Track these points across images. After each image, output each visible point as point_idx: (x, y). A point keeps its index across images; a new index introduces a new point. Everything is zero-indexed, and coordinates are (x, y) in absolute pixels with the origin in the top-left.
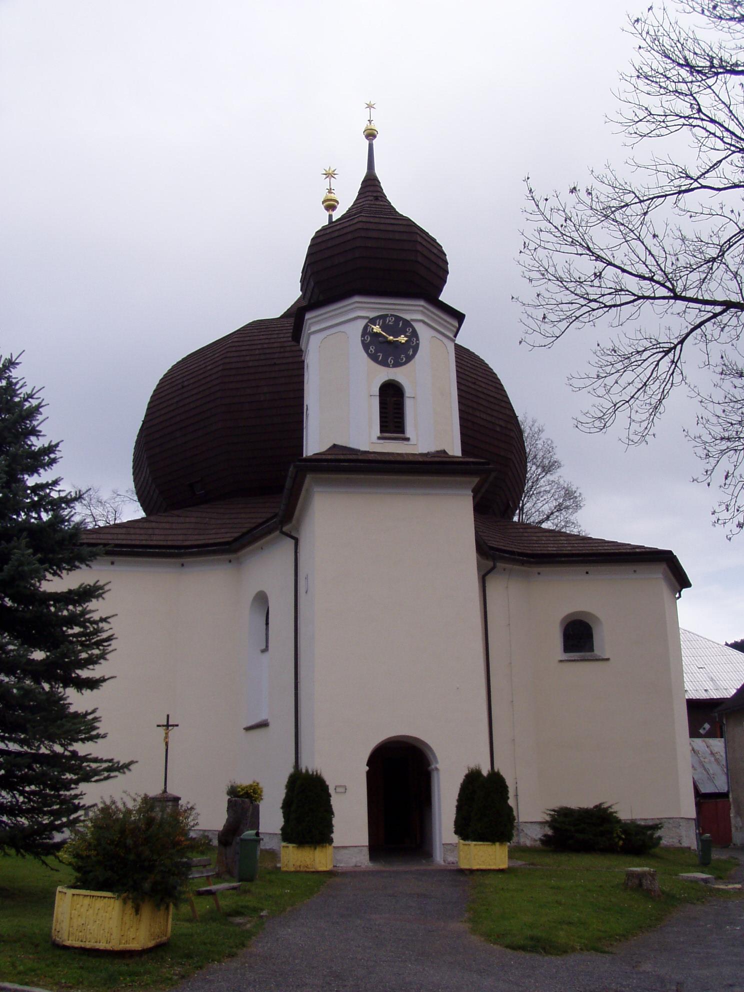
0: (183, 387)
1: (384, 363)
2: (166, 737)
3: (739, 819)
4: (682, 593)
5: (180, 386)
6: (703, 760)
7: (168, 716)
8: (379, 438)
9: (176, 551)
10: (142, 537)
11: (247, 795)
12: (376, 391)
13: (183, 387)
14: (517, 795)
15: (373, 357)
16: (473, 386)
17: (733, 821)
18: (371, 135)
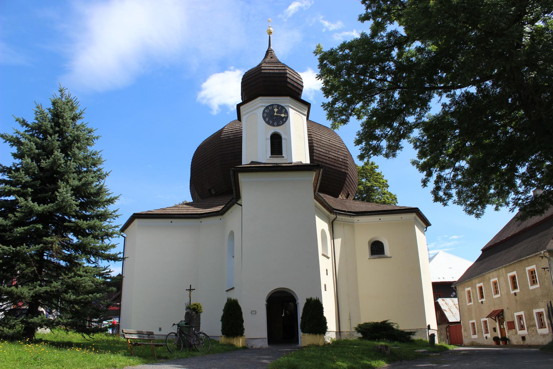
0: (205, 149)
1: (273, 125)
2: (190, 295)
3: (465, 333)
4: (427, 228)
5: (204, 149)
7: (191, 285)
8: (270, 157)
9: (520, 349)
10: (185, 211)
11: (194, 309)
12: (269, 137)
14: (350, 319)
15: (268, 123)
16: (328, 142)
17: (463, 334)
18: (270, 33)
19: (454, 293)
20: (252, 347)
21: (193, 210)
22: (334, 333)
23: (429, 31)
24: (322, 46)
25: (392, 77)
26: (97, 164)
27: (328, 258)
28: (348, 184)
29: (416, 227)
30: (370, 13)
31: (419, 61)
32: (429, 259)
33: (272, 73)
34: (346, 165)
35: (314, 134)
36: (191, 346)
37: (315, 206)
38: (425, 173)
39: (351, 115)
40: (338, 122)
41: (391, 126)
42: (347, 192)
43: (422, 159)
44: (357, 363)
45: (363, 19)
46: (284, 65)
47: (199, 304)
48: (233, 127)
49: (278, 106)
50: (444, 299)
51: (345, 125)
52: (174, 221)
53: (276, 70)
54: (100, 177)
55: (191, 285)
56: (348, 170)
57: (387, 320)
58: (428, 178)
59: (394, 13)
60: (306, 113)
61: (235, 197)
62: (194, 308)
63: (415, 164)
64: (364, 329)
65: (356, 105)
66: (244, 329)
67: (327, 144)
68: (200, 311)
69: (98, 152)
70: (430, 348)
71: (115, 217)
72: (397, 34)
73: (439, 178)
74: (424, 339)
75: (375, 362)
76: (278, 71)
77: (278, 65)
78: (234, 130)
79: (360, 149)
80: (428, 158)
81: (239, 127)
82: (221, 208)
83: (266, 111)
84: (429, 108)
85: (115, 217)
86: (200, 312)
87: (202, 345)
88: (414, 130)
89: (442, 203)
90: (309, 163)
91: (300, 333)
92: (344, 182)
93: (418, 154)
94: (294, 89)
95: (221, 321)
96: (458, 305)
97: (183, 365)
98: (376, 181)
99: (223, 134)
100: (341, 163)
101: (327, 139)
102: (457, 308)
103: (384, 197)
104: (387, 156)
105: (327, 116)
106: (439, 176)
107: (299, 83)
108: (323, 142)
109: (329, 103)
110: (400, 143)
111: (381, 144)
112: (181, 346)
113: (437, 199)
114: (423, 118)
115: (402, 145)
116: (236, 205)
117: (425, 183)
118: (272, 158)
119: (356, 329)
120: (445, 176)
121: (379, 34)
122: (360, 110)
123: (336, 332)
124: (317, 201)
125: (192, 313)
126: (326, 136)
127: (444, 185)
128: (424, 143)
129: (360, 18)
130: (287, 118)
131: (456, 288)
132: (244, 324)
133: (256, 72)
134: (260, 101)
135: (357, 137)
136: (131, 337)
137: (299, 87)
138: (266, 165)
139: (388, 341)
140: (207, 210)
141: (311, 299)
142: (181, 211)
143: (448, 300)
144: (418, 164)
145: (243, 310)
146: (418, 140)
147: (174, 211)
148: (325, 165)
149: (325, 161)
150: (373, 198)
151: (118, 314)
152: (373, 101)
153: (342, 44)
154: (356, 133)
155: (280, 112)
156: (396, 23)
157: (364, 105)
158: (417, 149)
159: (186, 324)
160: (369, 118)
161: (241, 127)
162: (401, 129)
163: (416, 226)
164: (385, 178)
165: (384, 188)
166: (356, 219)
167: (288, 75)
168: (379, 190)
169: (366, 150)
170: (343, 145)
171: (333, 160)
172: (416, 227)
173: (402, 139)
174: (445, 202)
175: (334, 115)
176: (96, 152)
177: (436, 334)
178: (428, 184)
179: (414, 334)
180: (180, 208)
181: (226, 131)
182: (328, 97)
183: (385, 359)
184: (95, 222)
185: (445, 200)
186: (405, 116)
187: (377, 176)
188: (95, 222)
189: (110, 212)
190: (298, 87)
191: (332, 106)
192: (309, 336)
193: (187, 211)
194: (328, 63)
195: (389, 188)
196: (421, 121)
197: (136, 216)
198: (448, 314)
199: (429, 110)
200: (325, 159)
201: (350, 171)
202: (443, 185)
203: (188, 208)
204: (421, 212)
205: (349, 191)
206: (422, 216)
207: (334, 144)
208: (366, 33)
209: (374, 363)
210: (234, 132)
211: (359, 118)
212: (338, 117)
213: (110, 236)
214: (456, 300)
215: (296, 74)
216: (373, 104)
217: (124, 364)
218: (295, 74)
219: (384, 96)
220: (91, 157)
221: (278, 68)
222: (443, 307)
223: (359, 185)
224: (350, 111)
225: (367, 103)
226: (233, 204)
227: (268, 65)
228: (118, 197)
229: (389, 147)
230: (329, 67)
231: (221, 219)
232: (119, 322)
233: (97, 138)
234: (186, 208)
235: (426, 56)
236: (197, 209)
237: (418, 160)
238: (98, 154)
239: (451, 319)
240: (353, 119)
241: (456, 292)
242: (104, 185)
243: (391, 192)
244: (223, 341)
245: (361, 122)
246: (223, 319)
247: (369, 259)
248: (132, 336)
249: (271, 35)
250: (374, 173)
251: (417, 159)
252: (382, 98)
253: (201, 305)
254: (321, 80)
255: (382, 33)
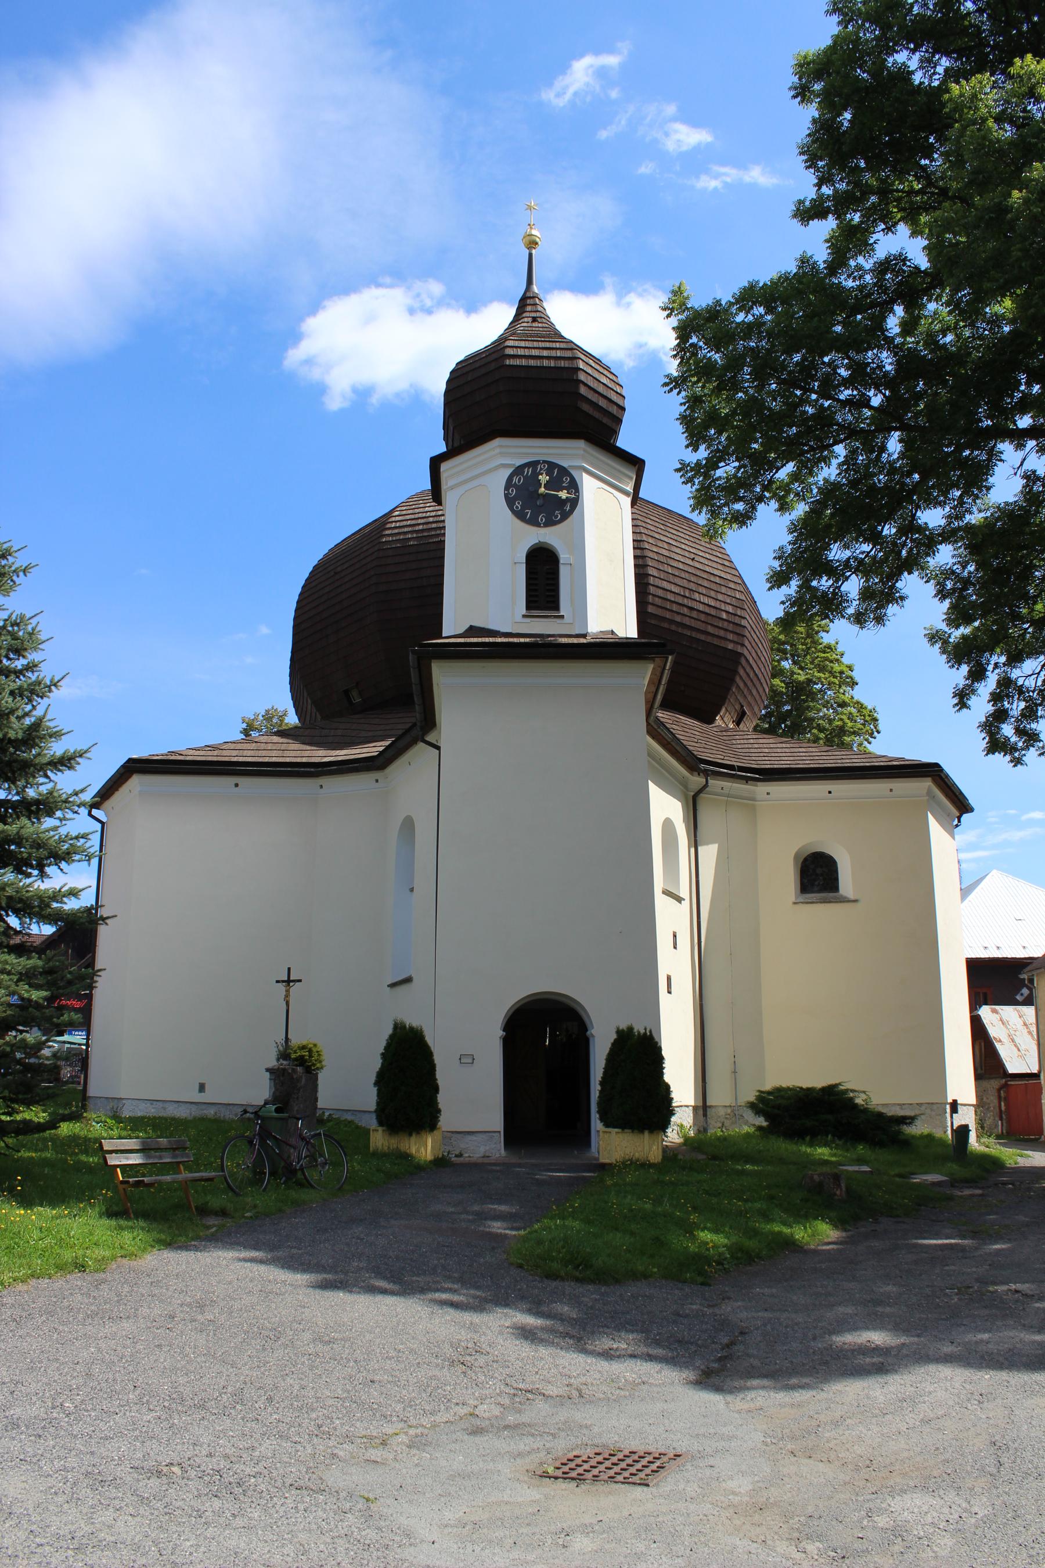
0: (336, 573)
1: (533, 522)
2: (287, 996)
6: (1013, 1032)
7: (289, 969)
10: (274, 753)
11: (301, 1061)
13: (336, 573)
14: (735, 1072)
15: (520, 515)
18: (532, 244)
19: (1025, 991)
20: (460, 1155)
21: (298, 753)
22: (690, 1111)
23: (1002, 281)
24: (687, 290)
25: (884, 395)
26: (26, 649)
27: (679, 900)
28: (741, 685)
29: (930, 817)
30: (829, 196)
31: (963, 349)
32: (961, 889)
33: (537, 367)
34: (738, 630)
35: (651, 540)
36: (291, 1172)
37: (650, 755)
38: (965, 669)
39: (760, 499)
40: (725, 520)
41: (875, 538)
42: (738, 707)
43: (957, 627)
44: (755, 1233)
45: (808, 213)
46: (569, 346)
47: (315, 1045)
48: (417, 511)
49: (551, 466)
50: (997, 1007)
51: (744, 527)
52: (244, 781)
53: (548, 358)
54: (35, 691)
55: (289, 969)
56: (743, 645)
57: (840, 1084)
58: (973, 683)
59: (899, 200)
60: (630, 488)
61: (418, 724)
62: (302, 1057)
63: (936, 642)
64: (773, 1107)
65: (776, 472)
66: (439, 1111)
67: (686, 568)
68: (318, 1065)
69: (28, 616)
70: (955, 1167)
71: (79, 806)
72: (904, 265)
73: (1005, 683)
74: (938, 1134)
75: (805, 1228)
76: (552, 364)
77: (554, 345)
78: (420, 521)
79: (783, 603)
80: (977, 624)
81: (433, 514)
82: (381, 749)
83: (515, 480)
84: (985, 487)
85: (79, 806)
86: (318, 1069)
87: (323, 1167)
88: (942, 547)
89: (1008, 758)
90: (636, 636)
91: (596, 1124)
92: (733, 680)
93: (946, 614)
94: (597, 415)
95: (376, 1084)
96: (1034, 1026)
97: (271, 1247)
98: (822, 669)
99: (387, 532)
100: (725, 625)
101: (687, 554)
102: (1032, 1035)
103: (842, 713)
104: (859, 619)
105: (692, 502)
106: (1004, 679)
107: (614, 397)
108: (675, 564)
109: (698, 463)
110: (899, 585)
111: (842, 589)
112: (265, 1173)
113: (996, 745)
114: (968, 517)
115: (905, 592)
116: (421, 745)
117: (962, 698)
118: (528, 620)
119: (752, 1106)
120: (1020, 682)
121: (852, 263)
122: (788, 485)
123: (695, 1109)
124: (653, 738)
125: (294, 1071)
126: (683, 546)
127: (1017, 707)
128: (966, 582)
129: (798, 209)
130: (575, 502)
131: (1031, 981)
132: (438, 1096)
133: (489, 363)
134: (498, 451)
135: (776, 564)
136: (125, 1162)
137: (614, 410)
138: (511, 640)
139: (838, 1142)
140: (338, 752)
141: (630, 1029)
142: (264, 753)
143: (1008, 1011)
144: (946, 642)
145: (437, 1059)
146: (949, 573)
147: (245, 753)
148: (680, 630)
149: (678, 619)
150: (811, 714)
151: (86, 1024)
152: (826, 461)
153: (745, 288)
154: (774, 551)
155: (554, 484)
156: (903, 229)
157: (800, 471)
158: (944, 599)
159: (277, 1110)
160: (812, 511)
161: (440, 513)
162: (904, 544)
163: (929, 814)
164: (846, 660)
165: (844, 687)
166: (761, 789)
167: (582, 377)
168: (829, 693)
169: (800, 606)
170: (734, 572)
171: (703, 617)
172: (930, 817)
173: (906, 574)
174: (1016, 755)
175: (714, 497)
176: (22, 617)
177: (972, 1127)
178: (973, 701)
179: (910, 1123)
180: (263, 746)
181: (398, 524)
182: (696, 450)
183: (833, 1214)
184: (22, 828)
185: (1016, 750)
186: (918, 507)
187: (824, 652)
188: (22, 828)
189: (64, 796)
190: (610, 410)
191: (706, 476)
192: (620, 1135)
193: (280, 753)
194: (701, 344)
195: (856, 687)
196: (961, 523)
197: (133, 767)
198: (1004, 1051)
199: (985, 492)
200: (678, 613)
201: (749, 647)
202: (1014, 706)
203: (283, 747)
204: (947, 776)
205: (744, 703)
206: (949, 788)
207: (707, 569)
208: (815, 258)
209: (799, 1233)
210: (421, 527)
211: (784, 507)
212: (724, 505)
213: (64, 859)
214: (1029, 1011)
215: (605, 372)
216: (826, 469)
217: (107, 1253)
218: (602, 370)
219: (858, 448)
220: (9, 631)
221: (553, 353)
222: (994, 1031)
223: (774, 676)
224: (758, 490)
225: (806, 470)
226: (413, 742)
227: (523, 344)
228: (86, 752)
229: (866, 594)
230: (705, 356)
231: (377, 781)
232: (87, 1045)
233: (24, 571)
234: (278, 746)
235: (986, 332)
236: (308, 748)
237: (946, 629)
238: (26, 625)
239: (1014, 1066)
240: (767, 511)
241: (1030, 990)
242: (48, 717)
243: (862, 701)
244: (379, 1144)
245: (788, 518)
246: (382, 1079)
247: (795, 903)
248: (127, 1159)
249: (534, 251)
250: (816, 643)
251: (943, 626)
252: (852, 454)
253: (320, 1047)
254: (679, 393)
255: (861, 260)
